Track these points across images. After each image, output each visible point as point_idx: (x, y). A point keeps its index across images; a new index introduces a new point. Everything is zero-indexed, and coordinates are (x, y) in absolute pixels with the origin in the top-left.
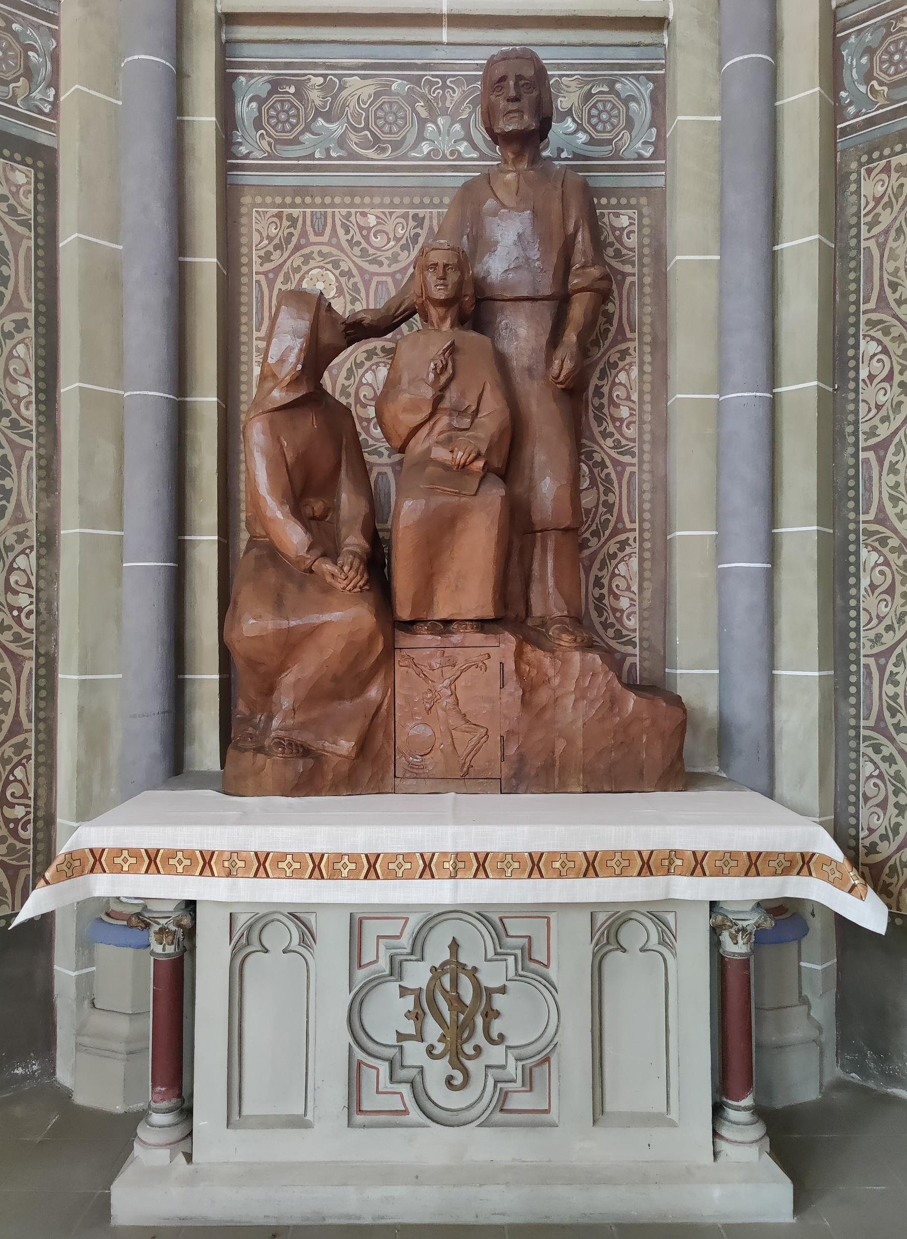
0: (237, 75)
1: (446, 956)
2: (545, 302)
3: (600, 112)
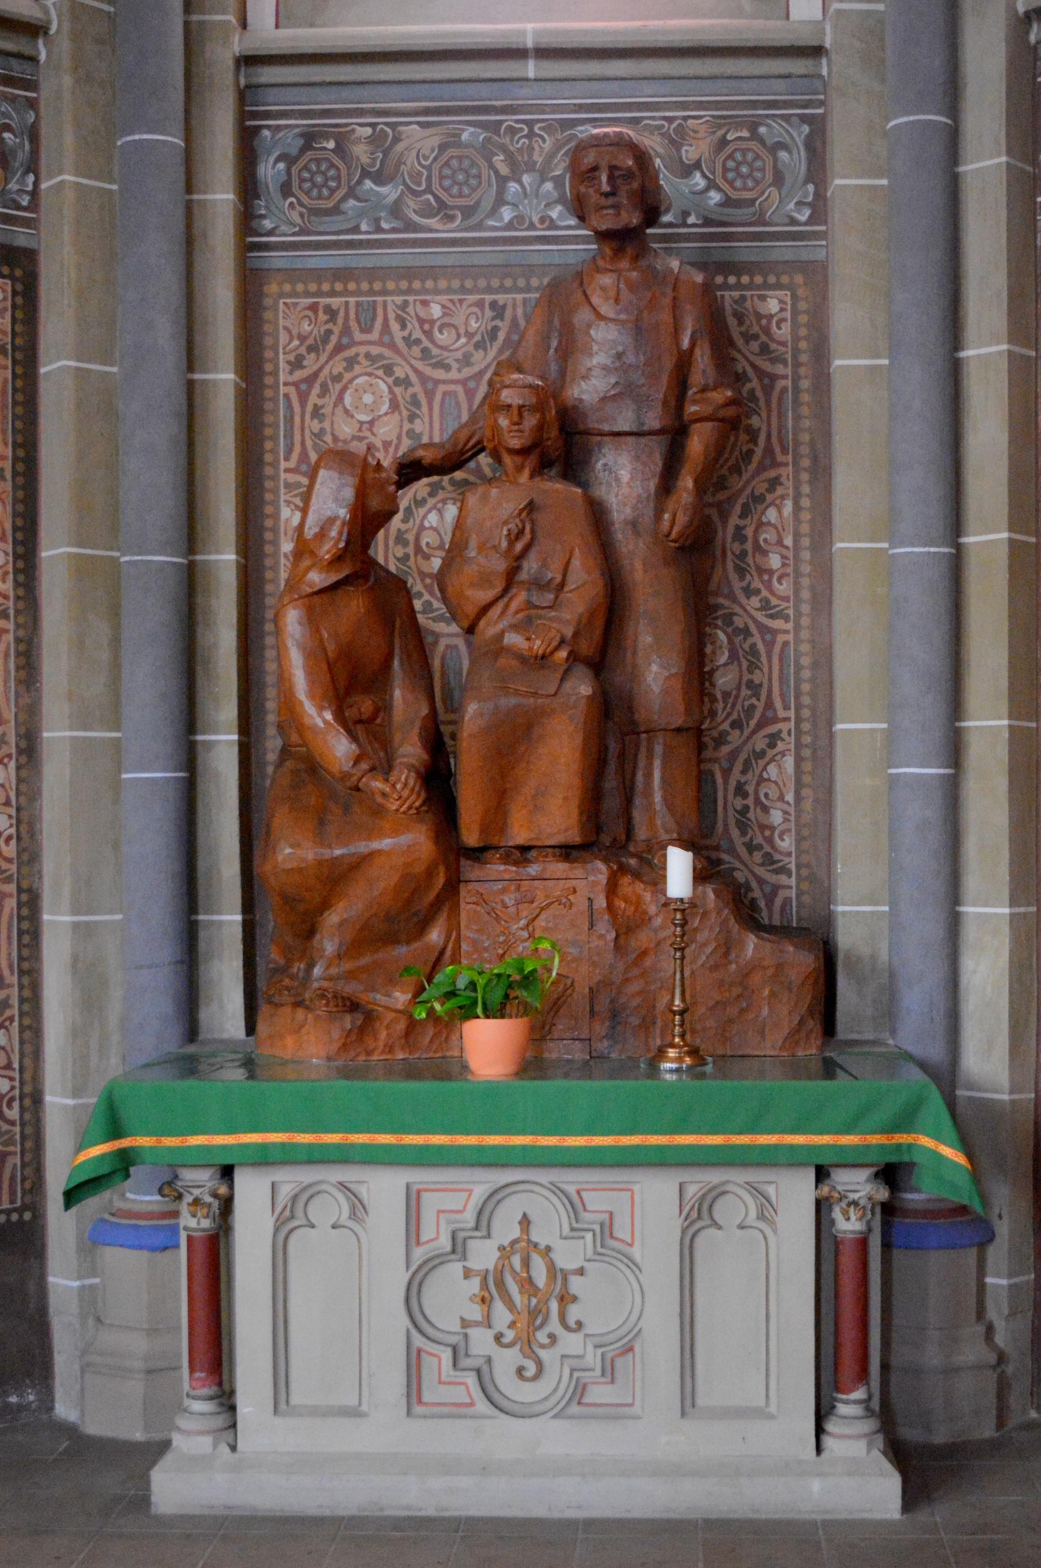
0: (261, 127)
1: (516, 1233)
2: (654, 437)
3: (739, 164)
